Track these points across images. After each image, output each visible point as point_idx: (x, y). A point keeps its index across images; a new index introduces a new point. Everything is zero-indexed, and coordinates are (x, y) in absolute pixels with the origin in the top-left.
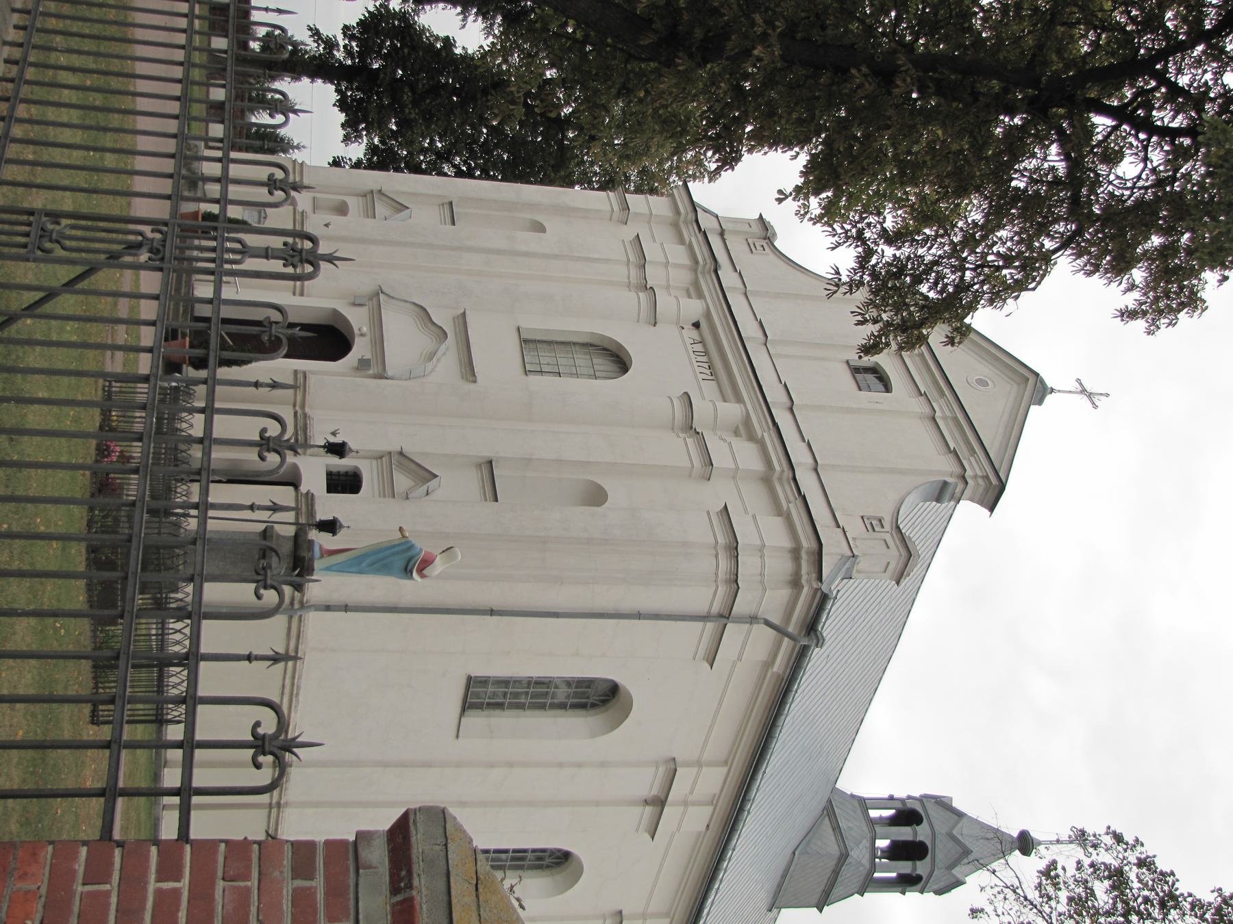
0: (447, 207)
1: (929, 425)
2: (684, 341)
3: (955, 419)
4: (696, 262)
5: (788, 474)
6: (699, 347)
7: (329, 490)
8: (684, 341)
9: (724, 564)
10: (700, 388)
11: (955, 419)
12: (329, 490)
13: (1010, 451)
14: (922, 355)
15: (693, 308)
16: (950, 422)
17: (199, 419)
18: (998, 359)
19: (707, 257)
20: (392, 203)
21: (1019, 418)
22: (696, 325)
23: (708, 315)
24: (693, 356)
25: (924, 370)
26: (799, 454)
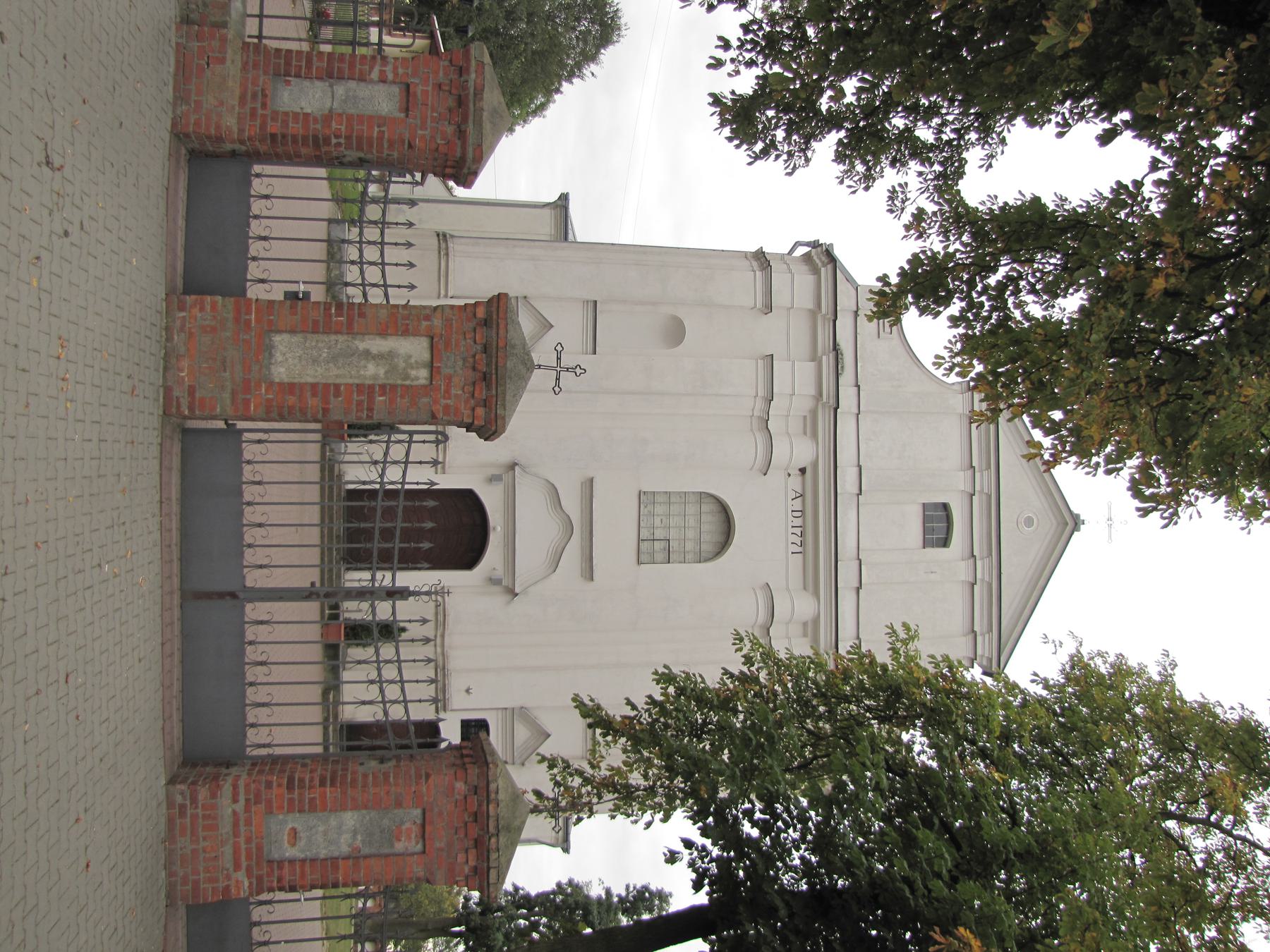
0: (591, 306)
1: (966, 501)
2: (786, 487)
3: (990, 585)
4: (821, 395)
5: (831, 316)
6: (797, 504)
7: (463, 721)
8: (786, 487)
9: (760, 404)
10: (787, 558)
11: (990, 585)
12: (463, 721)
13: (1018, 629)
14: (988, 431)
15: (804, 452)
16: (985, 584)
17: (355, 269)
18: (1051, 494)
19: (831, 394)
20: (539, 316)
21: (1041, 583)
22: (803, 471)
23: (815, 465)
24: (791, 518)
25: (985, 512)
26: (847, 393)
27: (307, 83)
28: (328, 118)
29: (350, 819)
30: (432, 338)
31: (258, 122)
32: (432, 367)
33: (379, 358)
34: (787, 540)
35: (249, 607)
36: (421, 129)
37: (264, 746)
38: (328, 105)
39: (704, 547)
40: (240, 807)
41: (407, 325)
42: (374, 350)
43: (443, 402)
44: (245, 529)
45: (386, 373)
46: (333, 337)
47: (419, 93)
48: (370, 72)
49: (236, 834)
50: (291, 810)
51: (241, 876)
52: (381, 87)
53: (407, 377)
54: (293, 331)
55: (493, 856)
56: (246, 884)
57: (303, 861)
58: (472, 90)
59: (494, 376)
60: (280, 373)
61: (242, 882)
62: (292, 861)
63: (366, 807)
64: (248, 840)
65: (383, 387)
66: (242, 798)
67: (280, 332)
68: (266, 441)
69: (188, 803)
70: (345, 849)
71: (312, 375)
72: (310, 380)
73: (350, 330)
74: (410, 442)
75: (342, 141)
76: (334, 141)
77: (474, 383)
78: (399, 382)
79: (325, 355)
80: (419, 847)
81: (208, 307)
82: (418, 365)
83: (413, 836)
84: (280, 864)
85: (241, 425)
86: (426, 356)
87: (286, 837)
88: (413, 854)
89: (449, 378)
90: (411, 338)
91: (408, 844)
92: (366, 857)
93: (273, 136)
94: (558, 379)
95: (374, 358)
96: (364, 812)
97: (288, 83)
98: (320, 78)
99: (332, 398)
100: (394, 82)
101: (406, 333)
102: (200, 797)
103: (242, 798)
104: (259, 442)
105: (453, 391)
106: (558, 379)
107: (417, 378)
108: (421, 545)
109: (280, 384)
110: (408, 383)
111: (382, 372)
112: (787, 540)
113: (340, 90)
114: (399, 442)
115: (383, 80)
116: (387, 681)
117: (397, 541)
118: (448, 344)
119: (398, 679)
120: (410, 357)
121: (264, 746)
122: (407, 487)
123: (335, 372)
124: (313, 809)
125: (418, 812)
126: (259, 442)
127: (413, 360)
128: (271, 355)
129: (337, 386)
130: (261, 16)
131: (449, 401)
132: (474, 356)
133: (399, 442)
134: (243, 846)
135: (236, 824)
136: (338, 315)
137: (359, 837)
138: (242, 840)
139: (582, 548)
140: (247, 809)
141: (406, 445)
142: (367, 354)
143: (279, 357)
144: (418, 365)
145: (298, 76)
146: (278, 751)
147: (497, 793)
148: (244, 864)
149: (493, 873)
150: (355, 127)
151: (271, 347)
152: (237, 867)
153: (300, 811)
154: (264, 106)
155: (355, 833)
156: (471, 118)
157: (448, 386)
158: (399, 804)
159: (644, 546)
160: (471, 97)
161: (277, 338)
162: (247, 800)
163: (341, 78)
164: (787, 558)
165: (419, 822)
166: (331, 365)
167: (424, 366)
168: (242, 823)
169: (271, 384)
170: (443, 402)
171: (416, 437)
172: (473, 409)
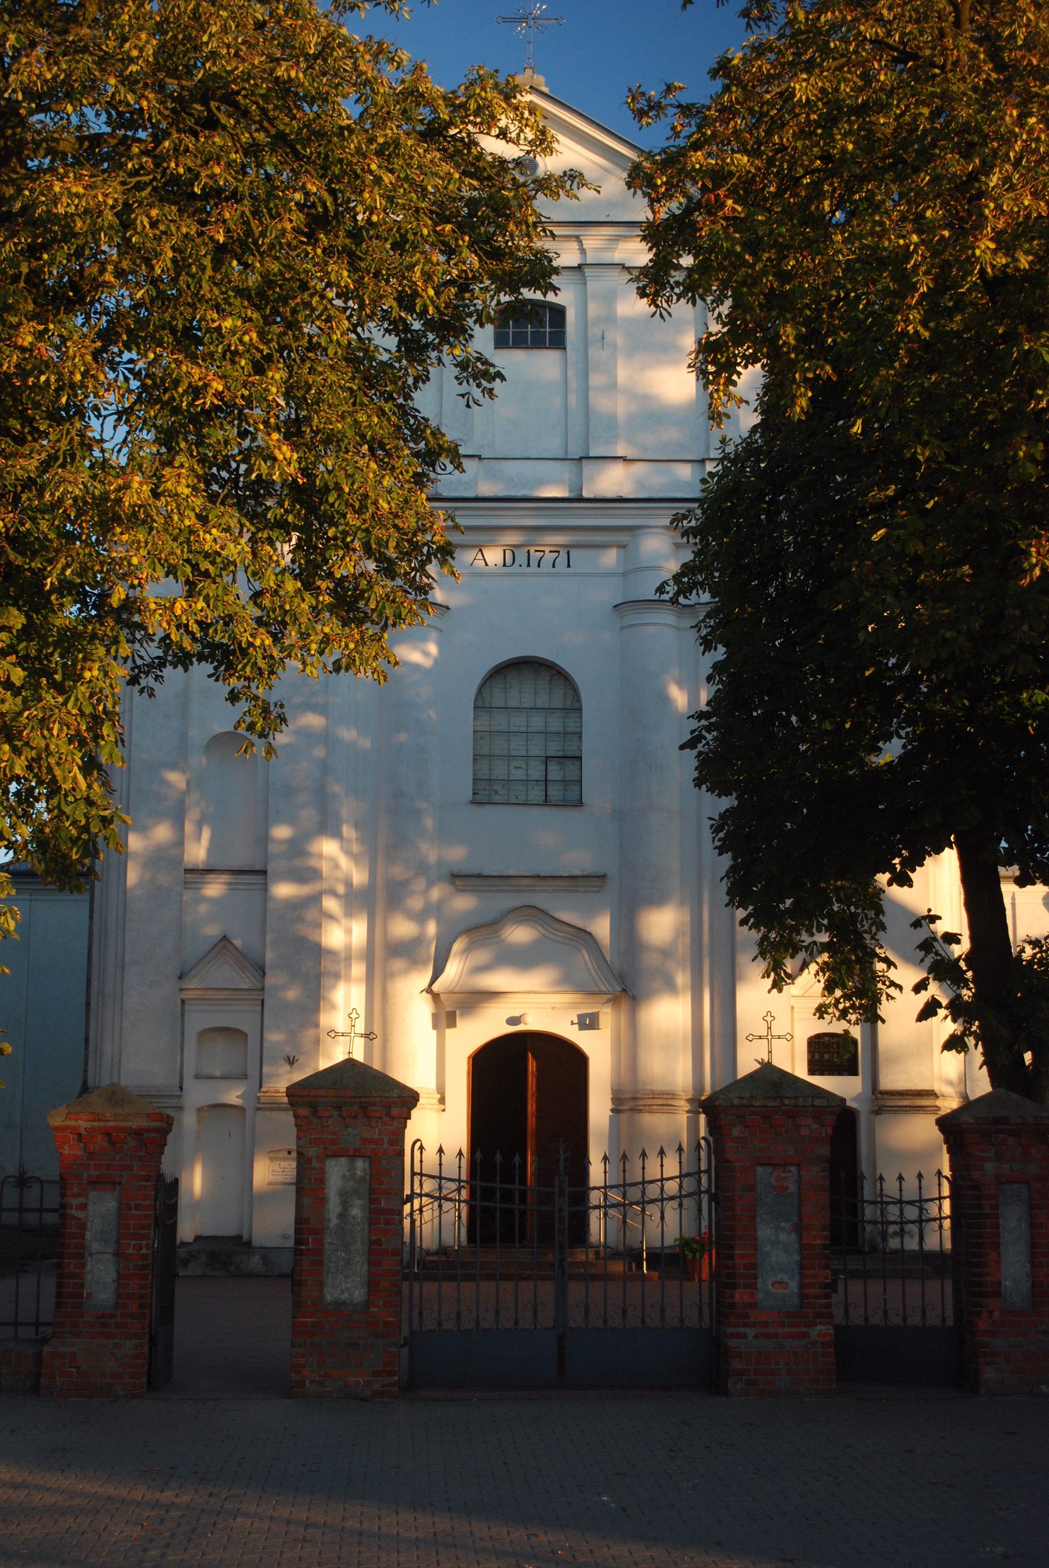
10: (576, 575)
27: (89, 1278)
28: (119, 1255)
29: (764, 1232)
30: (327, 1156)
31: (129, 1321)
32: (357, 1154)
33: (345, 1204)
34: (535, 575)
35: (572, 1324)
36: (132, 1170)
37: (701, 1311)
38: (109, 1256)
39: (558, 703)
40: (751, 1332)
41: (315, 1179)
42: (339, 1209)
43: (386, 1146)
44: (500, 1327)
45: (359, 1198)
46: (327, 1246)
47: (97, 1173)
48: (78, 1219)
49: (776, 1336)
50: (754, 1286)
51: (814, 1332)
52: (90, 1208)
53: (362, 1179)
54: (321, 1284)
55: (801, 1101)
56: (821, 1327)
57: (802, 1275)
58: (95, 1124)
59: (363, 1100)
60: (359, 1295)
61: (821, 1331)
62: (802, 1286)
63: (754, 1219)
64: (782, 1325)
65: (372, 1201)
66: (742, 1330)
67: (321, 1296)
68: (421, 1309)
69: (744, 1378)
70: (794, 1237)
71: (360, 1266)
72: (365, 1268)
73: (319, 1232)
74: (421, 1174)
75: (144, 1243)
76: (144, 1251)
77: (369, 1117)
78: (367, 1186)
79: (343, 1255)
80: (793, 1169)
81: (302, 1360)
82: (352, 1168)
83: (783, 1175)
84: (802, 1296)
85: (405, 1331)
86: (343, 1161)
87: (780, 1291)
88: (800, 1176)
89: (365, 1141)
90: (327, 1175)
91: (790, 1178)
92: (800, 1219)
93: (141, 1306)
94: (769, 1028)
95: (346, 1210)
96: (758, 1220)
97: (89, 1295)
98: (83, 1266)
99: (384, 1247)
100: (86, 1197)
101: (322, 1181)
102: (739, 1366)
103: (742, 1330)
104: (421, 1314)
105: (376, 1136)
106: (769, 1028)
107: (364, 1170)
108: (517, 1164)
109: (369, 1293)
110: (368, 1178)
111: (358, 1202)
112: (535, 575)
113: (95, 1246)
114: (421, 1185)
115: (84, 1207)
116: (643, 1196)
117: (512, 1187)
118: (333, 1142)
119: (641, 1186)
120: (344, 1177)
121: (701, 1311)
122: (464, 1177)
123: (358, 1246)
124: (754, 1266)
125: (759, 1169)
126: (421, 1314)
127: (348, 1174)
128: (344, 1303)
129: (371, 1243)
130: (16, 1324)
131: (386, 1141)
132: (344, 1118)
133: (421, 1185)
134: (787, 1330)
135: (767, 1336)
136: (307, 1243)
137: (782, 1224)
138: (780, 1330)
139: (468, 1072)
140: (753, 1325)
141: (424, 1178)
142: (342, 1216)
143: (345, 1296)
144: (352, 1168)
145: (82, 1286)
146: (706, 1299)
147: (742, 1098)
148: (803, 1329)
149: (818, 1102)
150: (132, 1231)
151: (338, 1304)
152: (806, 1335)
153: (756, 1277)
154: (112, 1316)
155: (778, 1228)
156: (122, 1124)
157: (371, 1141)
158: (752, 1188)
159: (555, 792)
160: (101, 1124)
161: (328, 1298)
162: (745, 1325)
163: (82, 1246)
164: (576, 575)
165: (769, 1169)
166: (352, 1248)
167: (352, 1163)
168: (765, 1331)
169: (368, 1304)
170: (386, 1146)
171: (417, 1169)
172: (393, 1118)
